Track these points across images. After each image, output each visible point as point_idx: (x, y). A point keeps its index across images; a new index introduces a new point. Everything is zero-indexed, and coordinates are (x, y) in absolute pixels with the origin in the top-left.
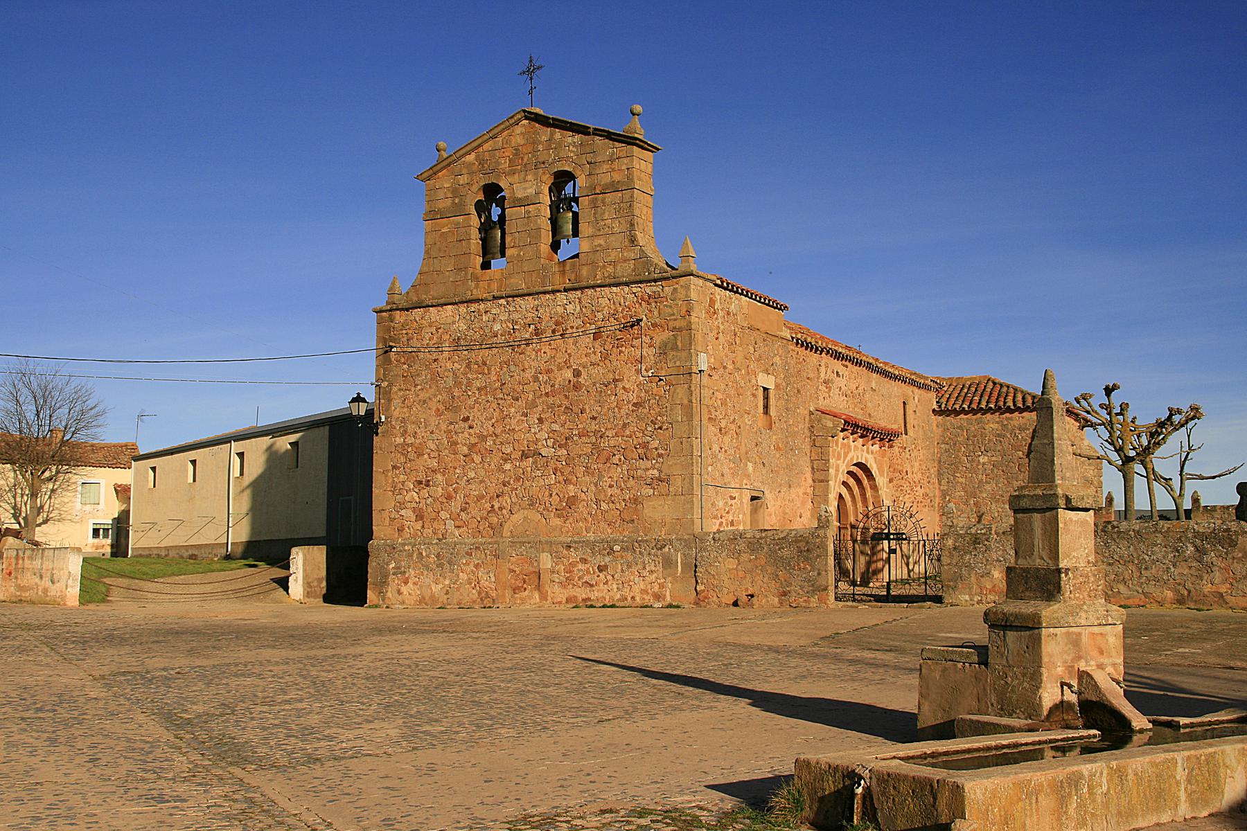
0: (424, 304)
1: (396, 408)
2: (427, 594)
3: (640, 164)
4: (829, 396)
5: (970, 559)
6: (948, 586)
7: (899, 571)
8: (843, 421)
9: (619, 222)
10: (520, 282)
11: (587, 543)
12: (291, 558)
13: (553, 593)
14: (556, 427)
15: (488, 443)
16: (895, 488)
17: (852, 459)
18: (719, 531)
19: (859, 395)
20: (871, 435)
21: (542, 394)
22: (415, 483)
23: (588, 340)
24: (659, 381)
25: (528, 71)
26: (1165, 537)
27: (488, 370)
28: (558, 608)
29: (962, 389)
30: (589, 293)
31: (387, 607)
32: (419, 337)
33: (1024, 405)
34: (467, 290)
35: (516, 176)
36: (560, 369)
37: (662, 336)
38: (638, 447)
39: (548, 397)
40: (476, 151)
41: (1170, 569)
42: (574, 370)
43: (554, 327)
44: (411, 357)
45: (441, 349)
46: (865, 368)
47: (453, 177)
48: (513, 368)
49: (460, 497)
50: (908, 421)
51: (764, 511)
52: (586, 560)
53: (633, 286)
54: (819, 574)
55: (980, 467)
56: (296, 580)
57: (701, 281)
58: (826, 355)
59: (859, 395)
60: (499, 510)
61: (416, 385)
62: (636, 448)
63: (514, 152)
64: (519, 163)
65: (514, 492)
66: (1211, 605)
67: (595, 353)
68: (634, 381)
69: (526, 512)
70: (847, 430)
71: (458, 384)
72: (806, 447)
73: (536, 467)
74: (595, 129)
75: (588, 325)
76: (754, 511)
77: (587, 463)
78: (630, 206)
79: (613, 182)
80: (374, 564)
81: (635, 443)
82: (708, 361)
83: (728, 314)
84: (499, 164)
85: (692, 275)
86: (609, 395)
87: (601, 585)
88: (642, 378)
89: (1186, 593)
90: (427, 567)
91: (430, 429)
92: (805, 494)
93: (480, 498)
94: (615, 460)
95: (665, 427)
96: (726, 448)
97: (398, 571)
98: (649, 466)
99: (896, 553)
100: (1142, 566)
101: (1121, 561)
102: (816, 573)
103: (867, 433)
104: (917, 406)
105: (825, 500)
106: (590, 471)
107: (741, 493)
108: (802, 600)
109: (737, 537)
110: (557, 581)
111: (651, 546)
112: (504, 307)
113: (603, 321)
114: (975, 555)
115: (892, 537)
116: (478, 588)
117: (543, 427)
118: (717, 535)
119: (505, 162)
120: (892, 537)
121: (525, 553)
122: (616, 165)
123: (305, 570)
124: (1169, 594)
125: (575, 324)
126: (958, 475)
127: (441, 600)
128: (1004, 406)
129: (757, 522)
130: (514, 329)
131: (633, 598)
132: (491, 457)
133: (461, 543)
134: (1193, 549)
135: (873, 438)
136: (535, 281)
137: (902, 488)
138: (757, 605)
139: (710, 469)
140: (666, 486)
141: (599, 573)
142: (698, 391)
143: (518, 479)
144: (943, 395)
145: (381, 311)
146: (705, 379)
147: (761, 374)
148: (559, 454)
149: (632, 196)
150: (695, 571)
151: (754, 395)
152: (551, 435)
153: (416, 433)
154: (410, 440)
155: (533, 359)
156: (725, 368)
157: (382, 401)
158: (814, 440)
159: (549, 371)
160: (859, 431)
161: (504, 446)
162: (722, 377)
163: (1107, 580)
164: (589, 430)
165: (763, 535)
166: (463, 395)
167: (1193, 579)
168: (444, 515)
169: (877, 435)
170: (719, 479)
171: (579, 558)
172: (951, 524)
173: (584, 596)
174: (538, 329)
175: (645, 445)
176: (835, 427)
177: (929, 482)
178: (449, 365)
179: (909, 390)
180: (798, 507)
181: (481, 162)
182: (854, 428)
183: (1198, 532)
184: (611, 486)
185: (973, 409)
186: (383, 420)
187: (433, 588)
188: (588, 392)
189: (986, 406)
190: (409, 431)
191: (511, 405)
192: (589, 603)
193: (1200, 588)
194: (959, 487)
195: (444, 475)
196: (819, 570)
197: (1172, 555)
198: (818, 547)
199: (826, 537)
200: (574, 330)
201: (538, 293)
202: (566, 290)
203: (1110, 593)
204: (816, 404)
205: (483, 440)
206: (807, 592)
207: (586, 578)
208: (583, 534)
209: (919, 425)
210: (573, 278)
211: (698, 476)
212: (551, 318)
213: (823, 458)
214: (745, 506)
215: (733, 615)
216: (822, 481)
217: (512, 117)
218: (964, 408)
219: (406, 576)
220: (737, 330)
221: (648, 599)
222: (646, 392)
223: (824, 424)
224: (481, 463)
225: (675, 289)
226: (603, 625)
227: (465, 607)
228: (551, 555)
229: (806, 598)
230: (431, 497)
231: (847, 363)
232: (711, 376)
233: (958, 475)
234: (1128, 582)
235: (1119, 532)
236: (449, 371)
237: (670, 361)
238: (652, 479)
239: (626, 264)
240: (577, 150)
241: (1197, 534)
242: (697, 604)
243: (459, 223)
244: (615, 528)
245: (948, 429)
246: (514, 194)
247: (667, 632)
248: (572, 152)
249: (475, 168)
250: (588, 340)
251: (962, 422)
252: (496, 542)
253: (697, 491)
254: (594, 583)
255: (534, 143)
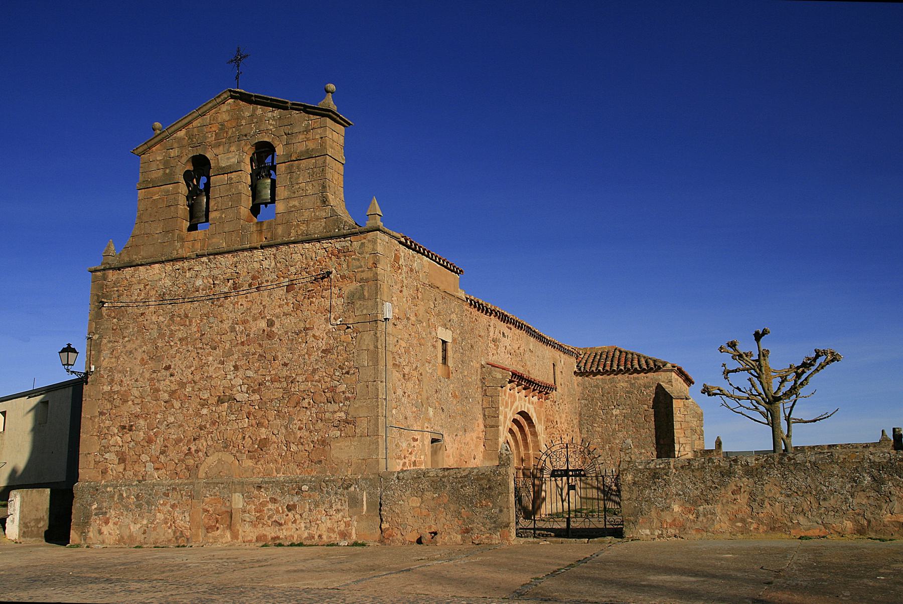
0: (134, 264)
1: (105, 359)
2: (126, 533)
3: (332, 135)
4: (497, 353)
5: (650, 494)
6: (629, 521)
7: (554, 505)
8: (511, 373)
9: (312, 184)
10: (221, 242)
11: (277, 483)
12: (9, 500)
13: (245, 532)
14: (250, 373)
15: (187, 390)
16: (549, 436)
17: (517, 408)
18: (402, 471)
19: (520, 354)
20: (533, 387)
21: (238, 343)
22: (119, 428)
23: (281, 292)
24: (346, 329)
25: (235, 60)
26: (841, 467)
27: (189, 321)
28: (248, 547)
29: (595, 357)
30: (284, 249)
31: (88, 547)
32: (129, 293)
33: (648, 367)
34: (174, 250)
35: (221, 148)
36: (255, 319)
37: (350, 287)
38: (327, 391)
39: (243, 346)
40: (186, 128)
41: (848, 499)
42: (268, 320)
43: (250, 281)
44: (120, 312)
45: (147, 303)
46: (525, 332)
47: (165, 150)
48: (211, 319)
49: (159, 441)
50: (557, 379)
51: (443, 454)
52: (275, 500)
53: (324, 242)
54: (501, 511)
55: (613, 418)
56: (13, 521)
57: (386, 237)
58: (495, 316)
59: (520, 354)
60: (195, 452)
61: (124, 337)
62: (324, 392)
63: (220, 127)
64: (224, 137)
65: (209, 436)
66: (892, 534)
67: (287, 304)
68: (323, 329)
69: (220, 454)
70: (514, 381)
71: (161, 335)
72: (479, 396)
73: (231, 411)
74: (293, 104)
75: (282, 278)
76: (434, 453)
77: (278, 407)
78: (323, 170)
79: (308, 149)
80: (78, 505)
81: (323, 387)
82: (393, 310)
83: (411, 270)
84: (205, 137)
85: (379, 230)
86: (300, 343)
87: (290, 523)
88: (331, 326)
89: (866, 523)
90: (127, 508)
91: (135, 377)
92: (478, 438)
93: (178, 441)
94: (305, 403)
95: (352, 372)
96: (409, 393)
97: (101, 512)
98: (336, 409)
99: (575, 489)
100: (820, 497)
101: (799, 493)
102: (497, 510)
103: (529, 385)
104: (563, 368)
105: (496, 443)
106: (281, 414)
107: (423, 436)
108: (484, 537)
109: (420, 476)
110: (248, 520)
111: (337, 486)
112: (206, 264)
113: (295, 274)
114: (655, 490)
115: (571, 473)
116: (174, 528)
117: (238, 374)
118: (401, 475)
119: (212, 136)
120: (571, 473)
121: (218, 494)
122: (310, 135)
123: (22, 511)
124: (849, 525)
125: (270, 278)
126: (596, 425)
127: (138, 539)
128: (632, 368)
129: (437, 463)
130: (214, 284)
131: (320, 536)
132: (189, 403)
133: (159, 485)
134: (869, 479)
135: (534, 390)
136: (235, 240)
137: (553, 435)
138: (440, 543)
139: (394, 411)
140: (352, 428)
141: (288, 513)
142: (383, 338)
143: (213, 423)
144: (581, 361)
145: (96, 271)
146: (390, 328)
147: (440, 328)
148: (253, 398)
149: (325, 162)
150: (380, 510)
151: (434, 346)
152: (245, 381)
153: (122, 381)
154: (116, 388)
155: (231, 311)
156: (408, 319)
157: (93, 352)
158: (485, 390)
159: (245, 322)
160: (523, 383)
161: (201, 393)
162: (406, 327)
163: (786, 511)
164: (280, 376)
165: (446, 473)
166: (165, 345)
167: (872, 508)
168: (144, 458)
169: (537, 388)
170: (403, 421)
171: (269, 497)
172: (629, 459)
173: (273, 535)
174: (236, 284)
175: (333, 389)
176: (503, 378)
177: (573, 431)
178: (154, 318)
179: (558, 354)
180: (472, 450)
181: (190, 136)
182: (519, 381)
183: (874, 462)
184: (300, 429)
185: (607, 371)
186: (93, 369)
187: (131, 528)
188: (280, 340)
189: (617, 368)
190: (115, 379)
191: (209, 354)
192: (278, 542)
193: (880, 518)
194: (597, 436)
195: (146, 420)
196: (501, 507)
197: (850, 486)
198: (500, 484)
199: (507, 474)
200: (269, 284)
201: (236, 251)
202: (262, 247)
203: (790, 524)
204: (486, 359)
205: (182, 387)
206: (490, 529)
207: (275, 518)
208: (273, 475)
209: (565, 384)
210: (269, 236)
211: (383, 418)
212: (248, 273)
213: (494, 406)
214: (427, 448)
215: (419, 555)
216: (492, 427)
217: (219, 97)
218: (599, 370)
219: (107, 516)
220: (419, 286)
221: (335, 538)
222: (335, 339)
223: (494, 376)
224: (180, 408)
225: (363, 244)
226: (284, 568)
227: (160, 546)
228: (243, 495)
229: (488, 535)
230: (134, 441)
231: (511, 326)
232: (396, 325)
233: (596, 425)
234: (807, 513)
235: (796, 464)
236: (154, 324)
237: (358, 309)
238: (339, 421)
239: (318, 223)
240: (276, 123)
241: (873, 464)
242: (382, 542)
243: (168, 191)
244: (304, 469)
245: (587, 388)
246: (219, 163)
247: (348, 578)
248: (271, 125)
249: (185, 142)
250: (281, 292)
251: (598, 381)
252: (192, 484)
253: (382, 432)
254: (283, 522)
255: (238, 119)
